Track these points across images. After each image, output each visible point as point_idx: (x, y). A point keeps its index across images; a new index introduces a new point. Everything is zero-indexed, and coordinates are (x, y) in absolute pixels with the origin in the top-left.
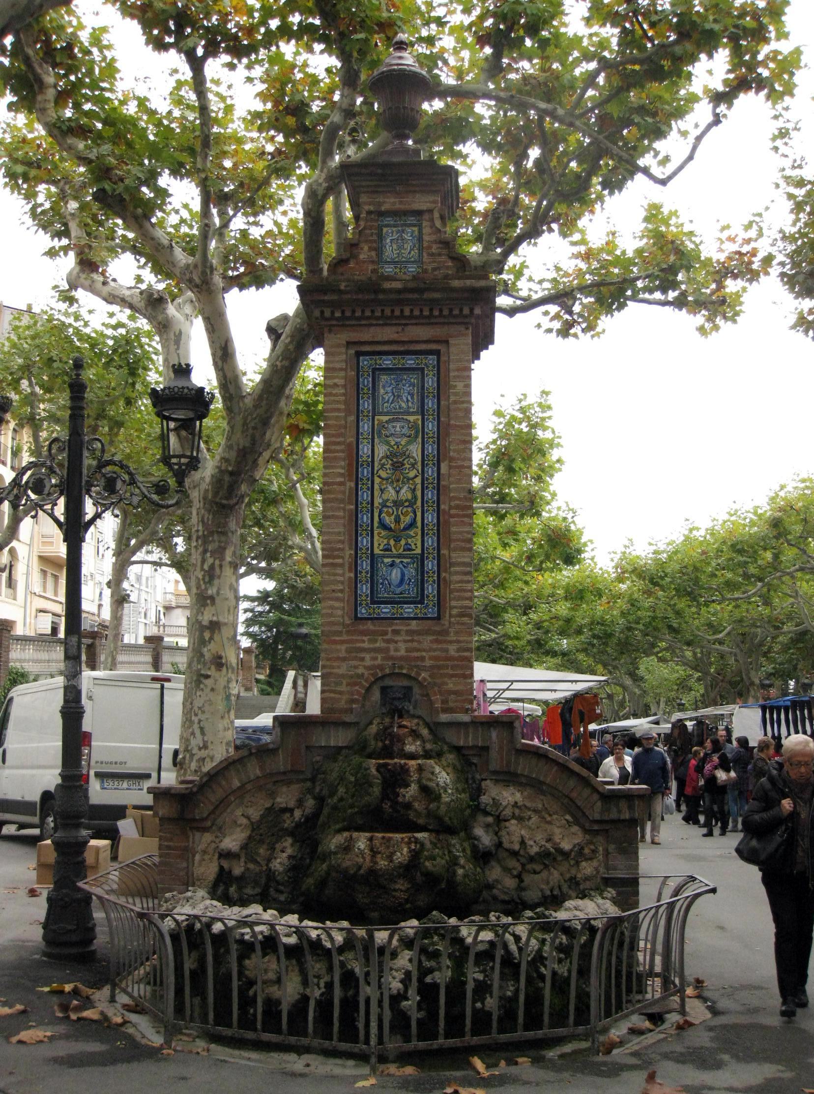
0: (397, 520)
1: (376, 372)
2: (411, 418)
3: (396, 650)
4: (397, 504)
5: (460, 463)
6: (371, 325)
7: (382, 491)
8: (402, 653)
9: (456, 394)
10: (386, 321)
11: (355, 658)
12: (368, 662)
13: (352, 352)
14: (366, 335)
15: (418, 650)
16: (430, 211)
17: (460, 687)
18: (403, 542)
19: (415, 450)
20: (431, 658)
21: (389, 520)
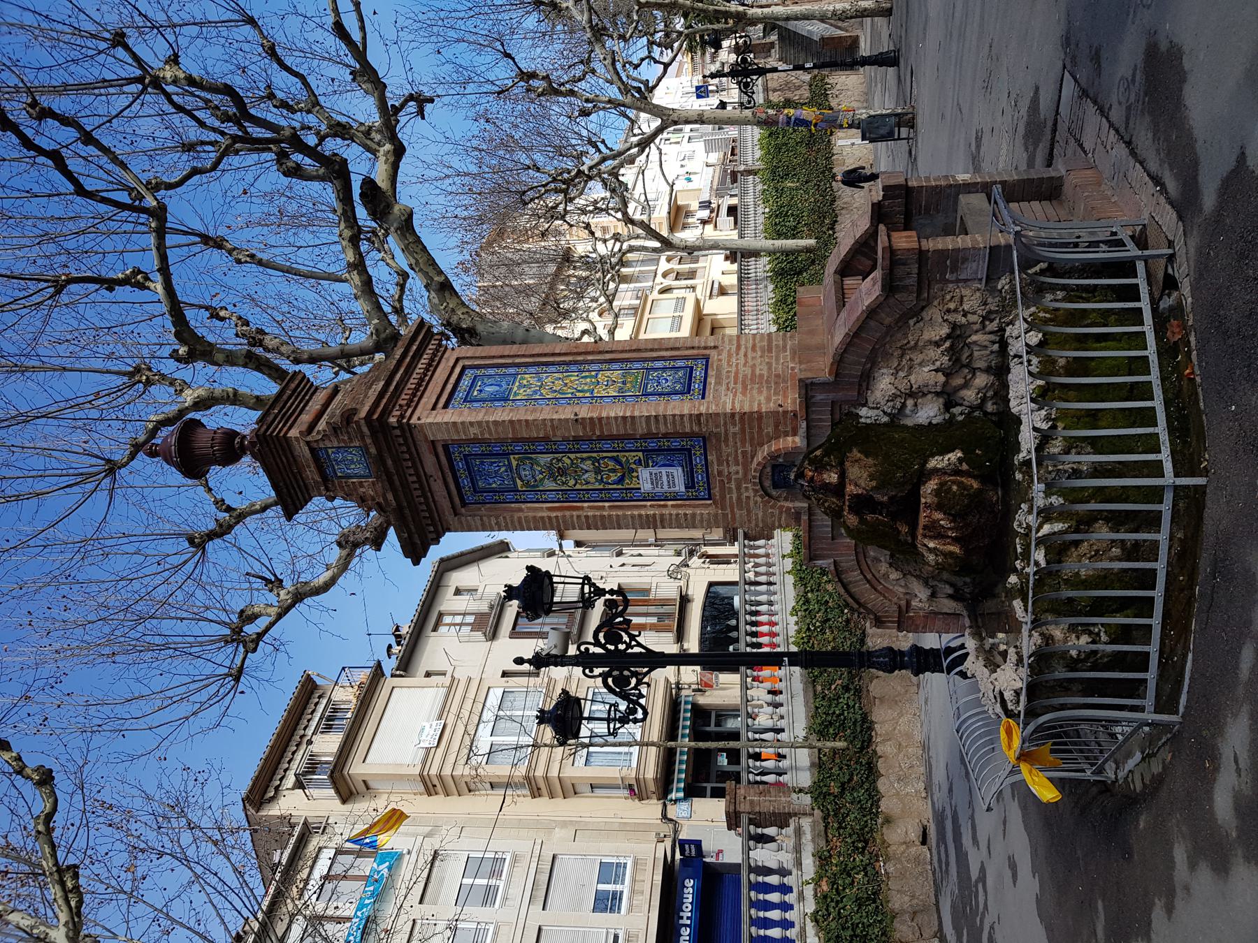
0: (614, 471)
1: (476, 490)
2: (514, 463)
3: (737, 473)
4: (598, 471)
5: (549, 428)
6: (434, 501)
7: (587, 483)
8: (740, 468)
9: (482, 434)
10: (426, 490)
11: (747, 504)
12: (751, 493)
13: (463, 510)
14: (445, 504)
15: (736, 456)
16: (308, 443)
17: (771, 421)
18: (634, 466)
19: (545, 459)
20: (744, 446)
21: (614, 477)
